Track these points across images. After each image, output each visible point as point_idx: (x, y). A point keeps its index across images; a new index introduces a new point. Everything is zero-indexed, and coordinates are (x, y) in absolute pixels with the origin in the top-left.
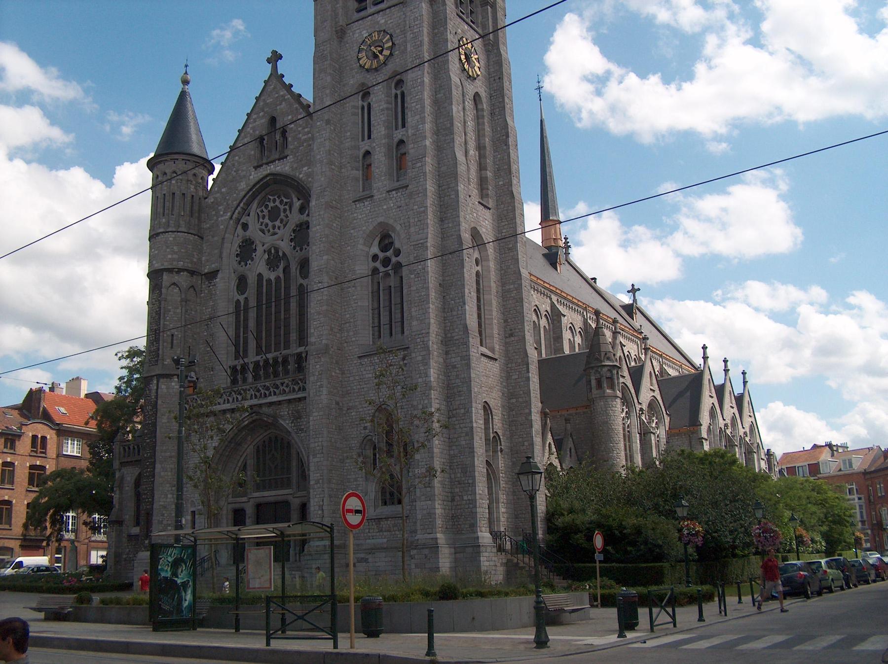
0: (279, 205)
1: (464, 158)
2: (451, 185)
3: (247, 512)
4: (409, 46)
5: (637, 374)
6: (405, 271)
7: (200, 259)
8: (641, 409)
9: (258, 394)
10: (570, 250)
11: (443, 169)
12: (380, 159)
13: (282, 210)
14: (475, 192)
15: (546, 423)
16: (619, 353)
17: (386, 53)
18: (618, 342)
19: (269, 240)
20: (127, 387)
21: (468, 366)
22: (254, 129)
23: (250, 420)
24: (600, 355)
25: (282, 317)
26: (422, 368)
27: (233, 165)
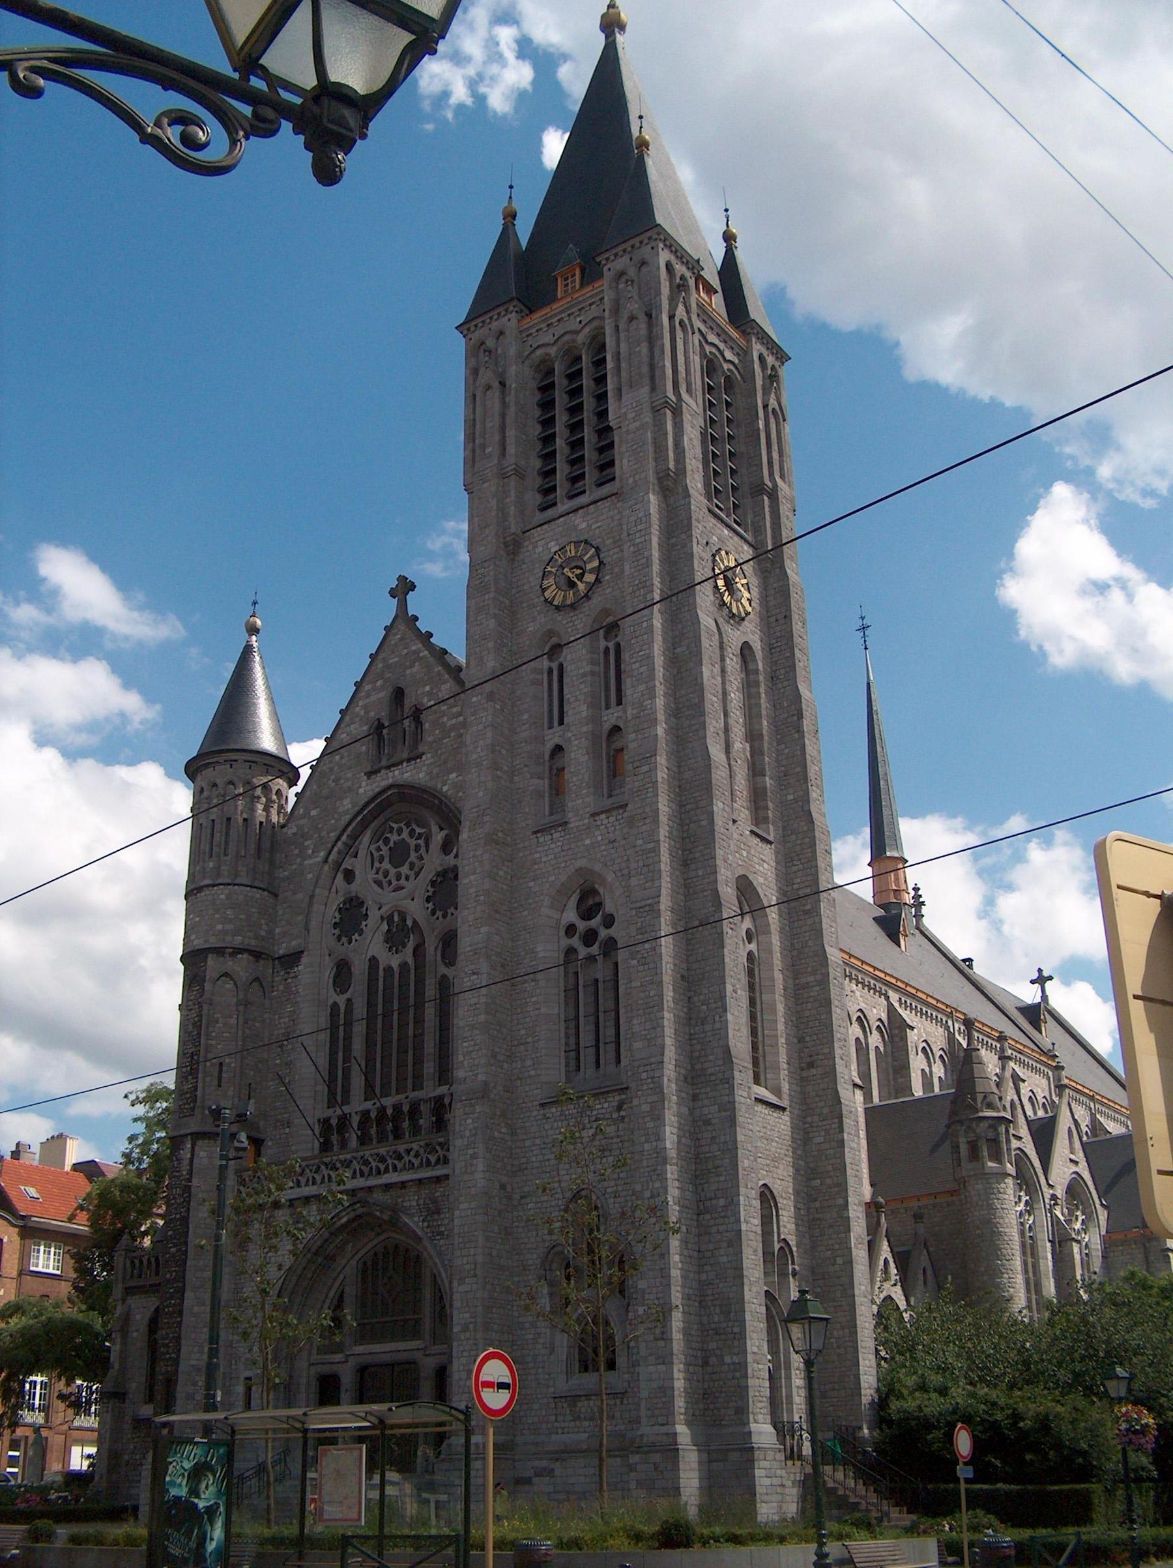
0: (408, 840)
1: (723, 757)
2: (702, 804)
3: (343, 1380)
4: (627, 567)
5: (1044, 1133)
6: (622, 955)
7: (271, 932)
8: (1054, 1197)
9: (366, 1170)
10: (924, 910)
11: (687, 775)
12: (580, 762)
13: (412, 847)
14: (744, 815)
15: (878, 1223)
16: (1011, 1095)
17: (590, 578)
18: (1008, 1074)
19: (391, 899)
20: (142, 1153)
21: (732, 1121)
22: (365, 707)
23: (352, 1215)
24: (974, 1100)
25: (411, 1033)
26: (651, 1125)
27: (331, 769)
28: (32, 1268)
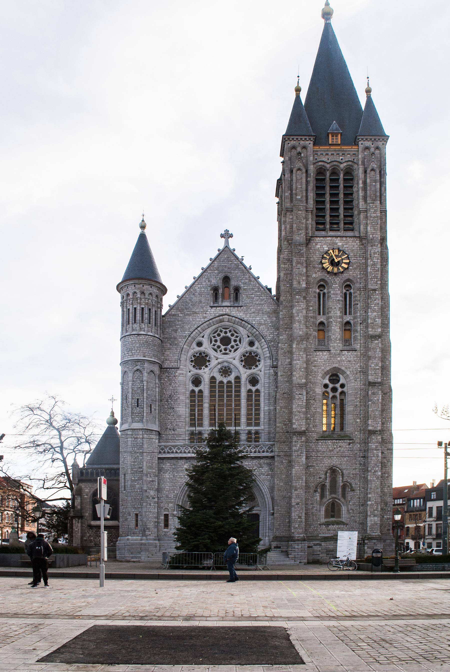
28: (435, 493)
